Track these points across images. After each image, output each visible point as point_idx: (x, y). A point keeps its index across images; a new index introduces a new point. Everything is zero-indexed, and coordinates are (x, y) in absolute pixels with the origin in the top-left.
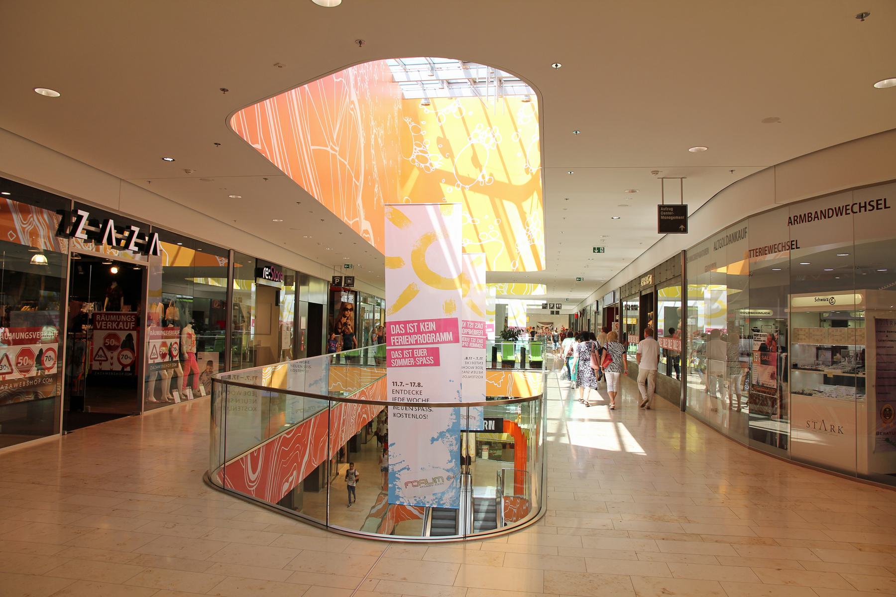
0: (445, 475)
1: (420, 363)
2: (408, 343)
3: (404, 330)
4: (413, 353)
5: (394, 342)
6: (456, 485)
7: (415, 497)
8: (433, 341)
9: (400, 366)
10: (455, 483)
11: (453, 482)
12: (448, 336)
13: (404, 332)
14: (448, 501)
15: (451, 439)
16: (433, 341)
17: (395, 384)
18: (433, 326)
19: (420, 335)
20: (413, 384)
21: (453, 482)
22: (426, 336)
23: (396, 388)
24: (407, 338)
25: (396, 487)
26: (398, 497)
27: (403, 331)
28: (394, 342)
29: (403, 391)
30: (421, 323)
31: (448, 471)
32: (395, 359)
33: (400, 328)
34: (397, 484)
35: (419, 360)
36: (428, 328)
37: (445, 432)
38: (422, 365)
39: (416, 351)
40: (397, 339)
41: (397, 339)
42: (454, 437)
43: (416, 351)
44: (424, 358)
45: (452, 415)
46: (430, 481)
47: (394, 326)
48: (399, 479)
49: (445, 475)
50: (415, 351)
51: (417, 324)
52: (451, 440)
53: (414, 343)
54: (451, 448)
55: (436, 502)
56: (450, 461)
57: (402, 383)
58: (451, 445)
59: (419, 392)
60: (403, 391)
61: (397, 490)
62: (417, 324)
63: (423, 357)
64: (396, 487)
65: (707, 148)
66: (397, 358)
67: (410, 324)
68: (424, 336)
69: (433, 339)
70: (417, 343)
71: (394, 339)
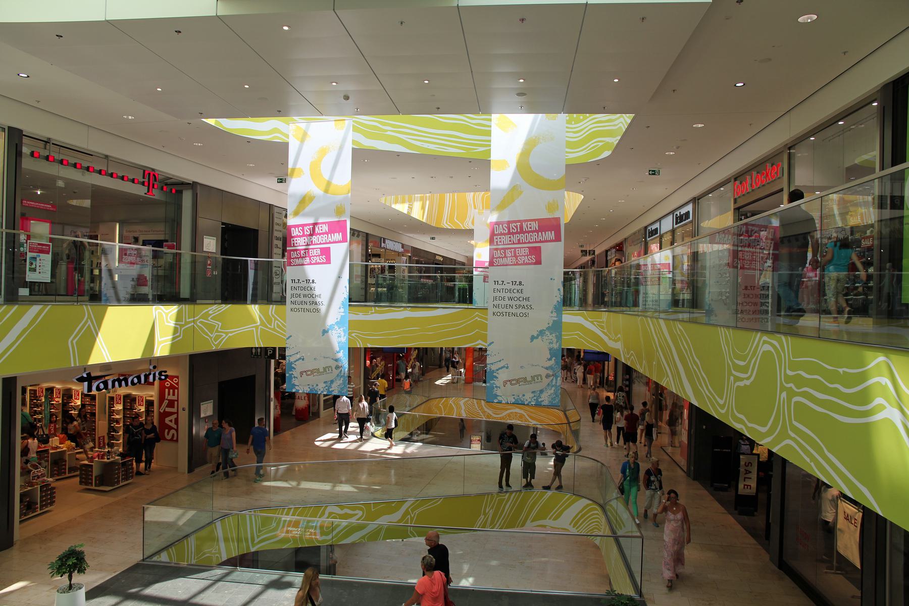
0: (544, 373)
1: (521, 262)
2: (510, 243)
3: (302, 232)
4: (515, 252)
5: (497, 242)
6: (556, 383)
7: (513, 395)
8: (536, 240)
9: (502, 265)
10: (554, 381)
11: (553, 380)
12: (550, 235)
13: (302, 234)
14: (546, 398)
15: (551, 337)
16: (536, 240)
17: (497, 283)
18: (535, 226)
19: (522, 235)
20: (514, 283)
21: (553, 380)
22: (320, 237)
23: (497, 287)
24: (510, 237)
25: (494, 386)
26: (294, 385)
27: (506, 231)
28: (497, 242)
29: (504, 290)
30: (524, 223)
31: (547, 368)
32: (293, 258)
33: (503, 228)
34: (495, 383)
35: (521, 259)
36: (322, 230)
37: (545, 330)
38: (316, 263)
39: (518, 251)
40: (500, 238)
41: (500, 238)
42: (342, 329)
43: (518, 251)
44: (526, 257)
45: (340, 308)
46: (529, 379)
47: (294, 229)
48: (497, 378)
49: (544, 373)
50: (310, 250)
51: (520, 224)
52: (339, 331)
53: (517, 242)
54: (340, 339)
55: (534, 400)
56: (550, 359)
57: (503, 282)
58: (339, 337)
59: (520, 291)
60: (504, 290)
61: (294, 379)
62: (520, 224)
63: (317, 256)
64: (293, 376)
65: (337, 83)
66: (296, 258)
67: (513, 224)
68: (526, 236)
69: (536, 238)
70: (519, 243)
71: (497, 239)
